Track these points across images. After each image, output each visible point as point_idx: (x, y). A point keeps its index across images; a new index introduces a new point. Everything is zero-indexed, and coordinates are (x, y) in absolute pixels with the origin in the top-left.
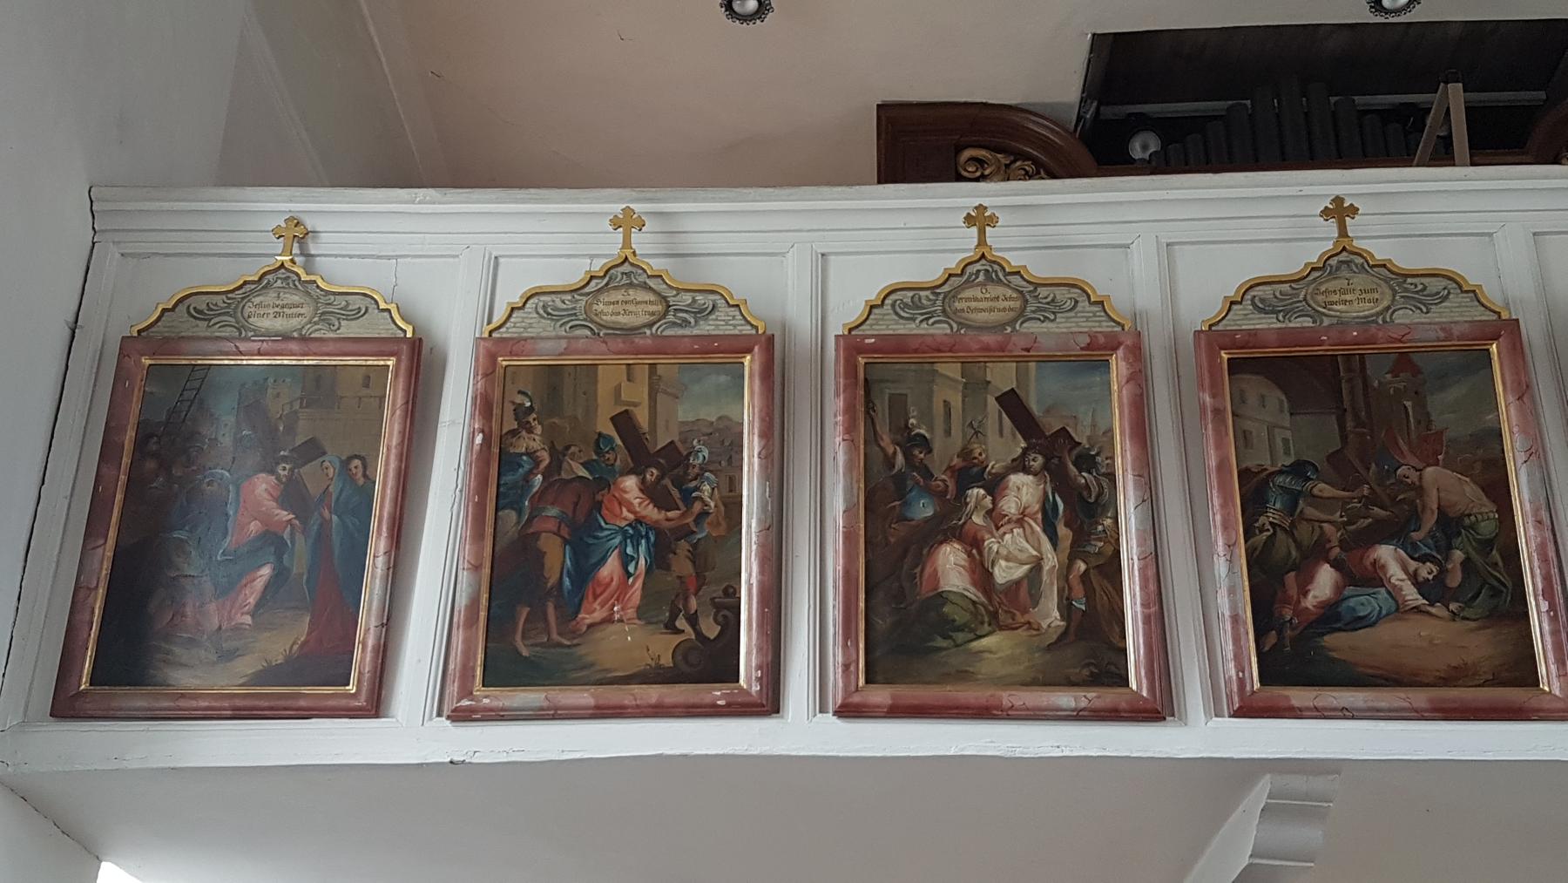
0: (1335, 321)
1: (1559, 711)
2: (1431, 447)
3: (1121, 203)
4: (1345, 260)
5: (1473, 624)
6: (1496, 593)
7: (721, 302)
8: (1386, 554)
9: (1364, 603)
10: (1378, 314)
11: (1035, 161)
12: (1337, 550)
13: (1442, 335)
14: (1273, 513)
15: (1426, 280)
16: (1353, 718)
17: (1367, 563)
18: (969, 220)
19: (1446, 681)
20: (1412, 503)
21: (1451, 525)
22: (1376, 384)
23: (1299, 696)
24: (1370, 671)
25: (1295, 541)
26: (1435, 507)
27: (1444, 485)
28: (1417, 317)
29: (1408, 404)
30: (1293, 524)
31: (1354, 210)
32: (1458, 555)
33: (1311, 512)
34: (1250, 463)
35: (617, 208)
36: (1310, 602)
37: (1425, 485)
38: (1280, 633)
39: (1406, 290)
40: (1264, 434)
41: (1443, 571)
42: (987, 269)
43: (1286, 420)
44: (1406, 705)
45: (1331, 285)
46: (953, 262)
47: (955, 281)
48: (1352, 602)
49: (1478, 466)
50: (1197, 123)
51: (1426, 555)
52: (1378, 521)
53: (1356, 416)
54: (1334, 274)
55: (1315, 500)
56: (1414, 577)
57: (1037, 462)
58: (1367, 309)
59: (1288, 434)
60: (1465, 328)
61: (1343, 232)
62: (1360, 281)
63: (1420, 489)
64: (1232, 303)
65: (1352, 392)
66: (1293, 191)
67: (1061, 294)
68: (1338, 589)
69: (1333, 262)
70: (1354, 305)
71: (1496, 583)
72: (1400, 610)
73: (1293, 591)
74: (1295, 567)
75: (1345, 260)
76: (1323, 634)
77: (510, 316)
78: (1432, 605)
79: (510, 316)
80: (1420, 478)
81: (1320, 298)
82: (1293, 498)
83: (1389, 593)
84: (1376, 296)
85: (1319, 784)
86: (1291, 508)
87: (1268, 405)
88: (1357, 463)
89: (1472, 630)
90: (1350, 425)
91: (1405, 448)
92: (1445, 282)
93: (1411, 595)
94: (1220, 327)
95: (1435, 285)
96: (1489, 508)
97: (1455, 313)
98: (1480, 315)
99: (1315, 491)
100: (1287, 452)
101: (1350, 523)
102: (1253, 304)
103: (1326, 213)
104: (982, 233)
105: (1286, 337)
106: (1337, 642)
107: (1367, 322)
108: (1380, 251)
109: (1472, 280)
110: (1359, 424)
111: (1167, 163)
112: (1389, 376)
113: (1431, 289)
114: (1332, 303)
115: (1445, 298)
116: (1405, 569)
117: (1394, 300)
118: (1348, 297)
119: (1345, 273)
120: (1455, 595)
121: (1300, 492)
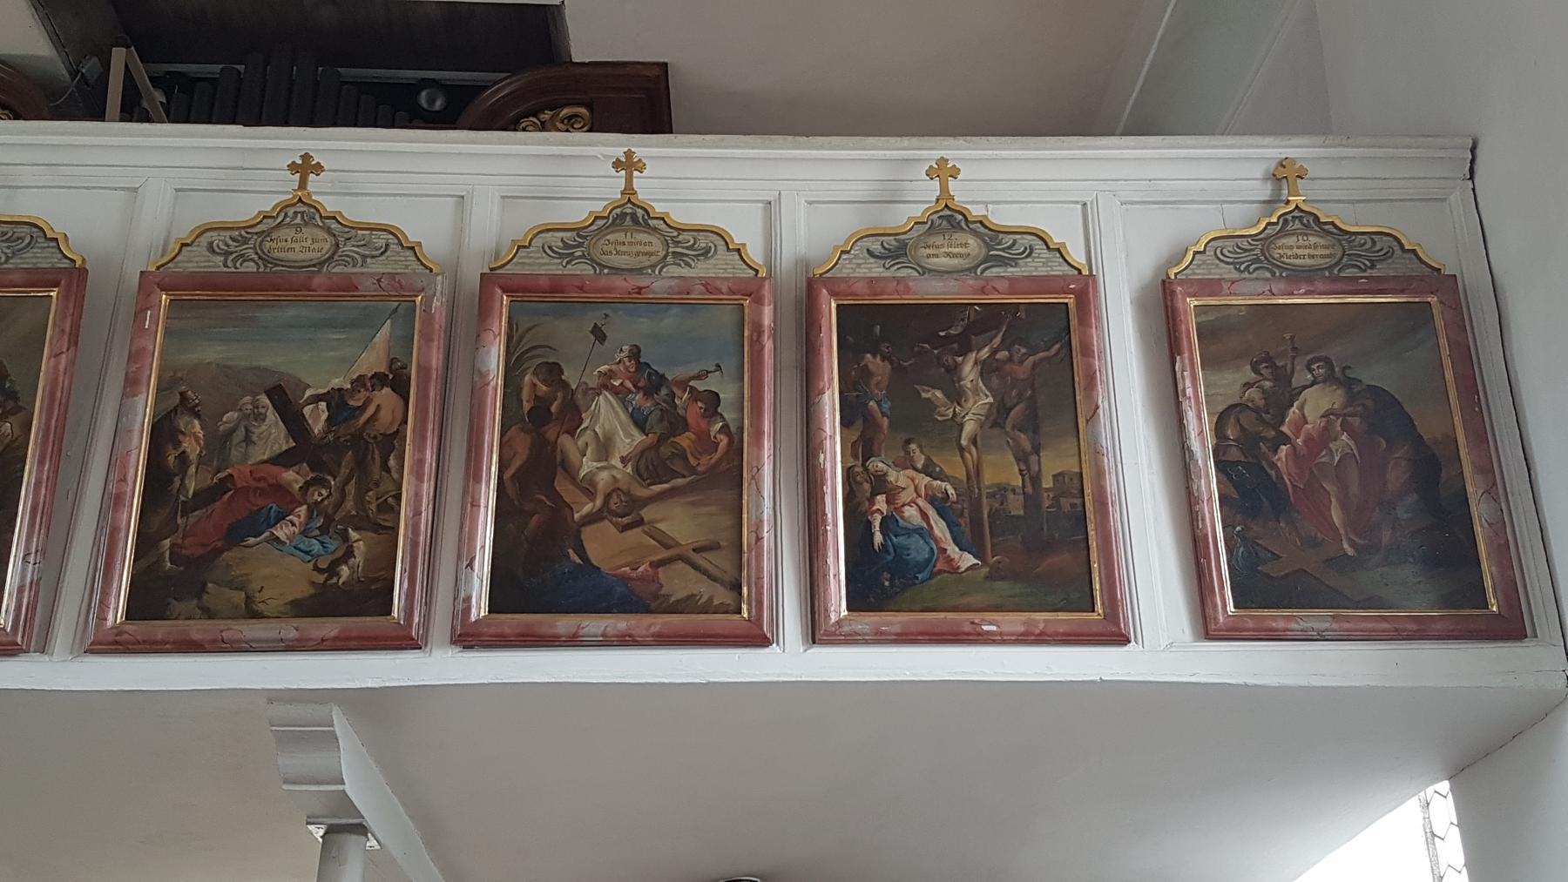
3: (562, 156)
4: (302, 212)
31: (319, 168)
35: (619, 152)
42: (630, 215)
46: (268, 204)
47: (271, 223)
50: (188, 84)
61: (303, 184)
64: (184, 245)
67: (21, 230)
70: (625, 249)
75: (302, 212)
92: (26, 229)
103: (293, 167)
104: (629, 180)
108: (330, 204)
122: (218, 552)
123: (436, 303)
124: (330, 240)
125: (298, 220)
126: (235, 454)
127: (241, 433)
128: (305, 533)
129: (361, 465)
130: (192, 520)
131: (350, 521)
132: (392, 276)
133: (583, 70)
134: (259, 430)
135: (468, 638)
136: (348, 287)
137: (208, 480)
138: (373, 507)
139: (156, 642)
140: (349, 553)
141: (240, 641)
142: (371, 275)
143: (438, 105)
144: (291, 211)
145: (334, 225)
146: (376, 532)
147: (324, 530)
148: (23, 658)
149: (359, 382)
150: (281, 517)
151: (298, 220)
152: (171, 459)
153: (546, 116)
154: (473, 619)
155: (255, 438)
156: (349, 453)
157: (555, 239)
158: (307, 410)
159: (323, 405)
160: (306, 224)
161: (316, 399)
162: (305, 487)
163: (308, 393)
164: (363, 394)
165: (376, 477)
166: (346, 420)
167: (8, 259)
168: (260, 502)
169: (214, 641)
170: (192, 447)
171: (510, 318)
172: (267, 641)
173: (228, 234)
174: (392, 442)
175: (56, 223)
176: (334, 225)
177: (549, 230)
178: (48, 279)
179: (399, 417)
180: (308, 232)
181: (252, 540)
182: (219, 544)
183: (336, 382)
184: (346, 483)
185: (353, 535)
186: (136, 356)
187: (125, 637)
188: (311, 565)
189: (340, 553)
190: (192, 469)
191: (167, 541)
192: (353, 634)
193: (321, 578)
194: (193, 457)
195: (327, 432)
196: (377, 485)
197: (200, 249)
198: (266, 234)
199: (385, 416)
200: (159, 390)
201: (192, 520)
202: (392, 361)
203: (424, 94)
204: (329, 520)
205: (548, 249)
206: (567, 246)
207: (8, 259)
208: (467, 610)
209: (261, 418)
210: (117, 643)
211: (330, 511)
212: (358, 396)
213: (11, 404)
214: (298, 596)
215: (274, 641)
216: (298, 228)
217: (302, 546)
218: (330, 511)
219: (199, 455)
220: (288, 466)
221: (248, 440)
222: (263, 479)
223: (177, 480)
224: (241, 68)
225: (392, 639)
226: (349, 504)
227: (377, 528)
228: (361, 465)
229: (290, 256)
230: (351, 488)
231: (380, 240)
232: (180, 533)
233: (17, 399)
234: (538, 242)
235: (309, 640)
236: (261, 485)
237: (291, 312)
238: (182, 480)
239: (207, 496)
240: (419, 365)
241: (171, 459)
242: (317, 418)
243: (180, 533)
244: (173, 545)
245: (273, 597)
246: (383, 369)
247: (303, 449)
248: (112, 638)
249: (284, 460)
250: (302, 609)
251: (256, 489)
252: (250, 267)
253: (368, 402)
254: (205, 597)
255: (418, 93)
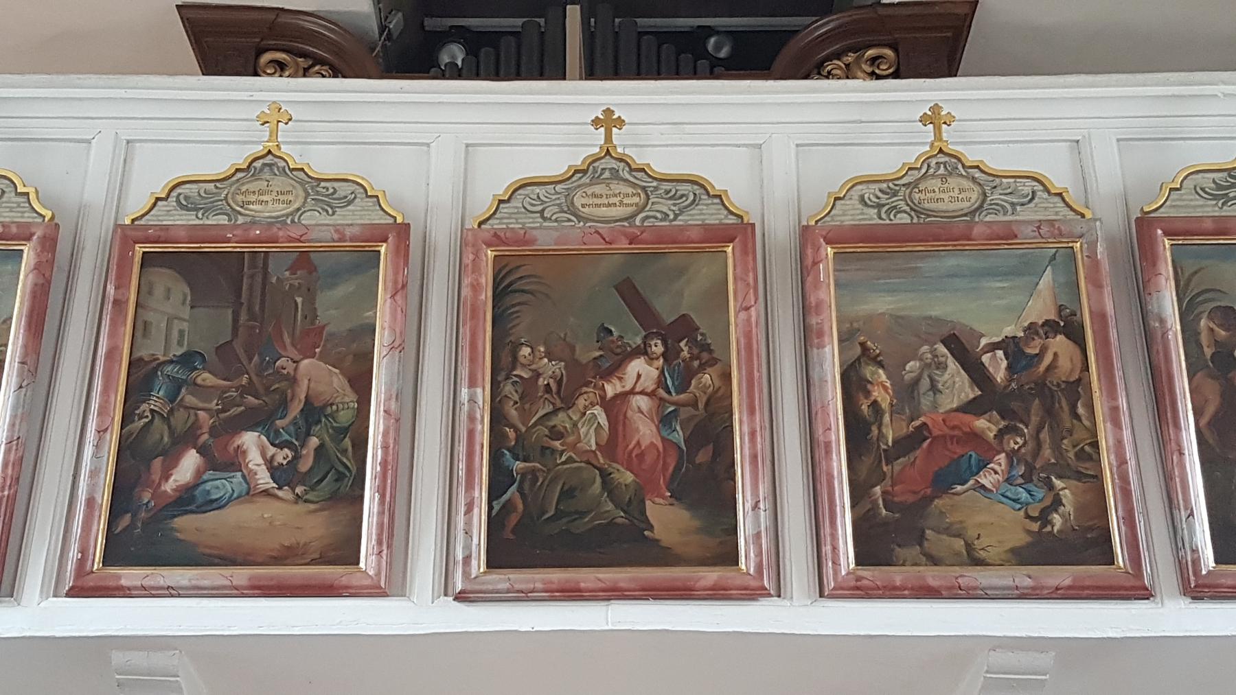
0: (249, 219)
1: (367, 587)
2: (311, 339)
4: (266, 165)
5: (312, 507)
6: (340, 477)
7: (361, 195)
8: (250, 440)
9: (221, 486)
10: (287, 215)
11: (332, 67)
12: (206, 436)
13: (336, 236)
14: (156, 401)
15: (336, 185)
16: (179, 596)
17: (231, 449)
18: (924, 120)
19: (276, 560)
20: (284, 393)
21: (314, 413)
22: (274, 280)
23: (130, 575)
24: (208, 551)
25: (169, 427)
26: (303, 397)
27: (316, 376)
28: (324, 219)
29: (299, 300)
30: (171, 411)
31: (620, 122)
32: (314, 441)
33: (190, 400)
34: (144, 353)
36: (169, 486)
37: (298, 377)
38: (134, 516)
39: (318, 193)
40: (163, 325)
41: (297, 457)
43: (186, 312)
44: (227, 583)
45: (252, 186)
47: (916, 175)
48: (208, 486)
49: (350, 357)
50: (492, 38)
51: (287, 441)
52: (251, 410)
53: (250, 309)
54: (256, 176)
55: (195, 387)
56: (269, 463)
57: (657, 348)
58: (279, 210)
59: (185, 326)
60: (355, 231)
62: (279, 183)
63: (293, 380)
65: (251, 287)
66: (244, 96)
67: (684, 188)
68: (199, 473)
69: (258, 164)
70: (267, 205)
71: (341, 469)
72: (251, 493)
73: (156, 476)
74: (164, 453)
75: (946, 163)
76: (175, 516)
77: (155, 205)
78: (280, 488)
79: (155, 205)
80: (296, 369)
81: (240, 198)
82: (177, 386)
83: (244, 476)
84: (290, 198)
85: (159, 659)
86: (172, 397)
87: (172, 296)
88: (241, 352)
89: (315, 511)
90: (243, 317)
91: (287, 340)
92: (688, 187)
93: (264, 479)
94: (142, 222)
95: (344, 190)
96: (351, 398)
97: (356, 217)
98: (379, 219)
99: (199, 381)
100: (180, 344)
101: (223, 411)
102: (178, 201)
103: (596, 122)
104: (938, 132)
105: (196, 234)
106: (187, 525)
107: (280, 222)
109: (718, 186)
110: (252, 317)
111: (695, 73)
112: (287, 273)
113: (341, 193)
114: (249, 203)
115: (350, 203)
116: (263, 455)
117: (305, 202)
118: (265, 198)
119: (266, 175)
120: (303, 479)
121: (185, 381)
122: (928, 500)
123: (1100, 249)
124: (976, 188)
125: (942, 171)
126: (926, 402)
127: (925, 382)
128: (1009, 480)
129: (1050, 412)
130: (897, 468)
131: (1047, 467)
132: (1051, 223)
133: (890, 11)
134: (943, 378)
135: (1199, 589)
136: (1007, 235)
137: (905, 429)
138: (1071, 455)
139: (895, 588)
140: (1057, 502)
141: (975, 588)
142: (1029, 222)
143: (723, 54)
144: (933, 162)
145: (978, 174)
146: (1079, 480)
147: (1027, 477)
148: (764, 602)
149: (1031, 329)
150: (982, 465)
151: (942, 171)
152: (865, 407)
153: (850, 58)
154: (1204, 572)
155: (940, 386)
156: (1036, 399)
157: (1207, 181)
158: (986, 359)
159: (1000, 353)
160: (951, 174)
161: (993, 347)
162: (1000, 434)
163: (984, 342)
164: (1038, 342)
165: (1068, 425)
166: (1025, 368)
167: (676, 216)
168: (960, 451)
169: (950, 588)
170: (882, 396)
171: (1173, 261)
172: (1004, 588)
173: (876, 186)
174: (1077, 388)
175: (377, 181)
176: (978, 174)
177: (1028, 177)
178: (720, 235)
179: (1079, 365)
180: (953, 182)
181: (959, 488)
182: (929, 491)
183: (1009, 330)
184: (1039, 430)
185: (1058, 483)
186: (806, 309)
187: (865, 582)
188: (1022, 513)
189: (1048, 502)
190: (887, 418)
191: (878, 489)
192: (1087, 583)
193: (1035, 527)
194: (885, 405)
195: (1010, 381)
196: (1070, 432)
197: (1187, 194)
198: (914, 185)
199: (1064, 364)
200: (840, 341)
201: (897, 468)
202: (1060, 309)
203: (712, 40)
204: (1030, 469)
205: (1199, 191)
206: (1219, 187)
207: (676, 216)
208: (1196, 562)
209: (942, 367)
210: (858, 588)
211: (1029, 459)
212: (1032, 344)
213: (705, 356)
214: (1018, 544)
215: (1009, 588)
216: (943, 178)
217: (1008, 494)
218: (1029, 459)
219: (892, 405)
220: (979, 414)
221: (934, 388)
222: (954, 428)
223: (875, 429)
224: (542, 21)
225: (1126, 589)
226: (1047, 452)
227: (1079, 476)
228: (1050, 412)
229: (940, 206)
230: (1045, 435)
231: (1027, 187)
232: (888, 481)
233: (711, 352)
234: (1189, 184)
235: (1043, 588)
236: (956, 432)
237: (951, 262)
238: (879, 428)
239: (907, 444)
240: (1091, 312)
241: (865, 407)
242: (997, 366)
243: (888, 481)
244: (884, 493)
245: (992, 544)
246: (1052, 316)
247: (989, 398)
248: (853, 583)
249: (972, 407)
250: (1021, 557)
251: (952, 437)
252: (904, 219)
253: (1044, 349)
254: (926, 544)
255: (711, 36)
